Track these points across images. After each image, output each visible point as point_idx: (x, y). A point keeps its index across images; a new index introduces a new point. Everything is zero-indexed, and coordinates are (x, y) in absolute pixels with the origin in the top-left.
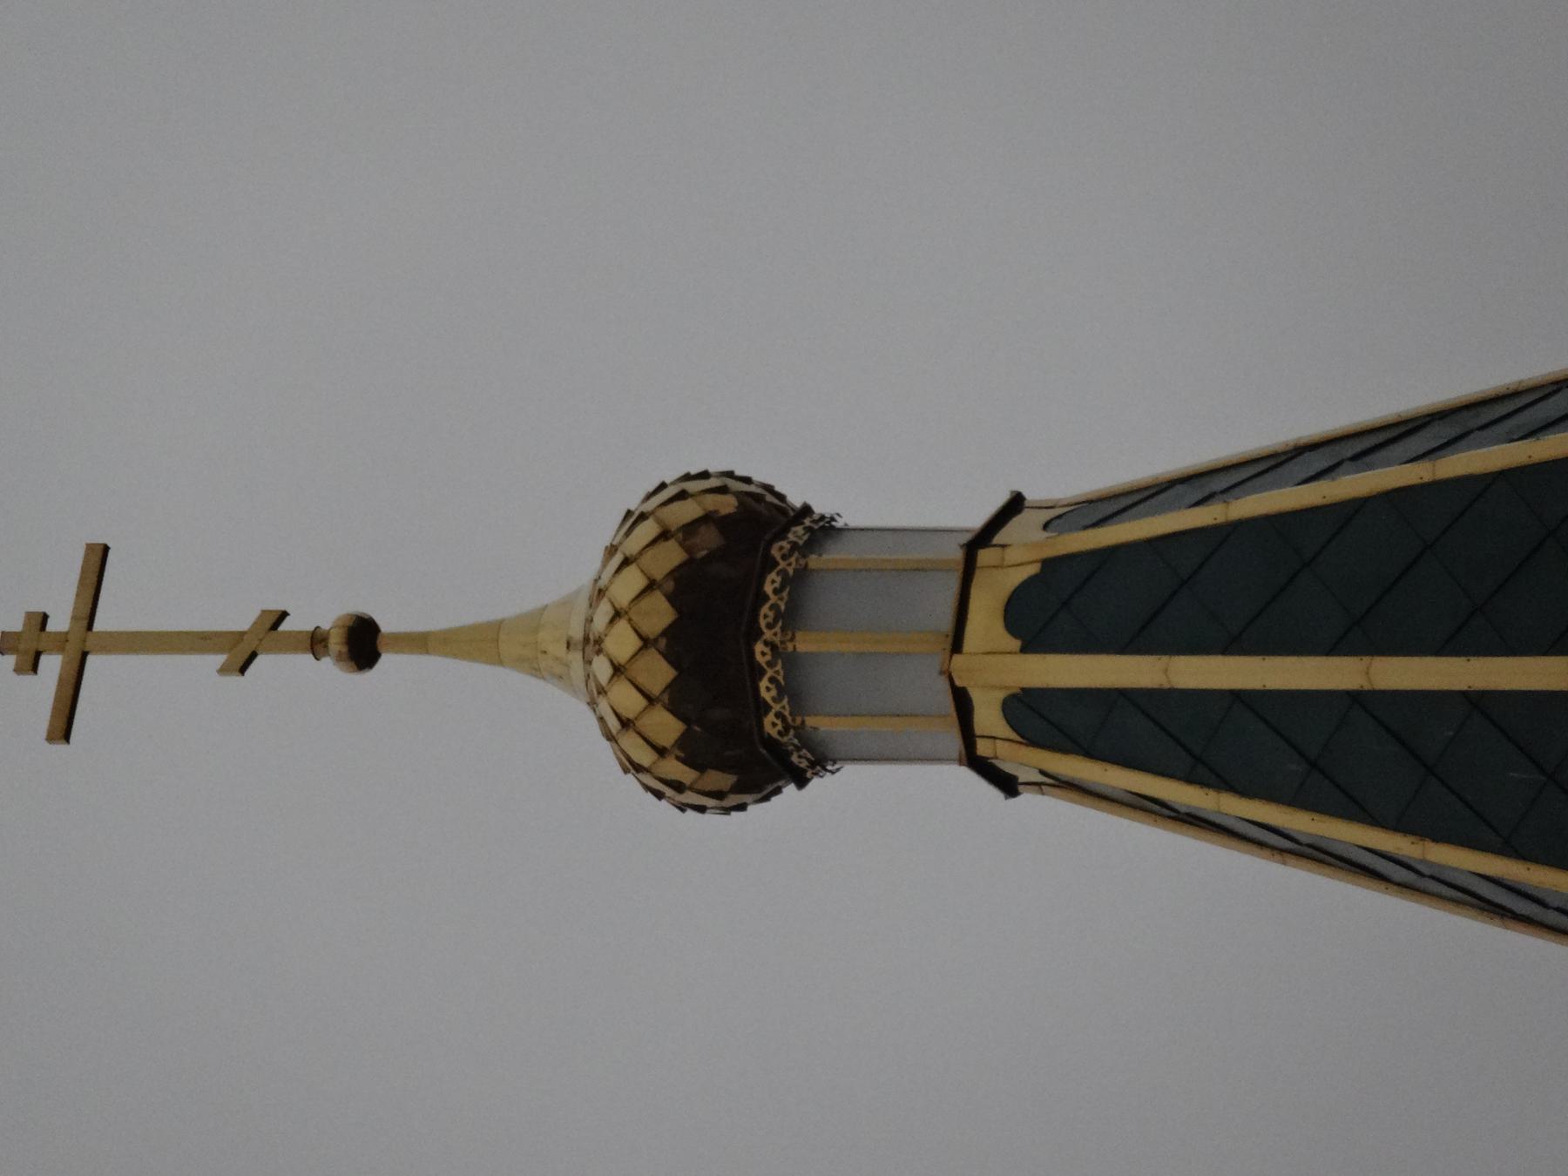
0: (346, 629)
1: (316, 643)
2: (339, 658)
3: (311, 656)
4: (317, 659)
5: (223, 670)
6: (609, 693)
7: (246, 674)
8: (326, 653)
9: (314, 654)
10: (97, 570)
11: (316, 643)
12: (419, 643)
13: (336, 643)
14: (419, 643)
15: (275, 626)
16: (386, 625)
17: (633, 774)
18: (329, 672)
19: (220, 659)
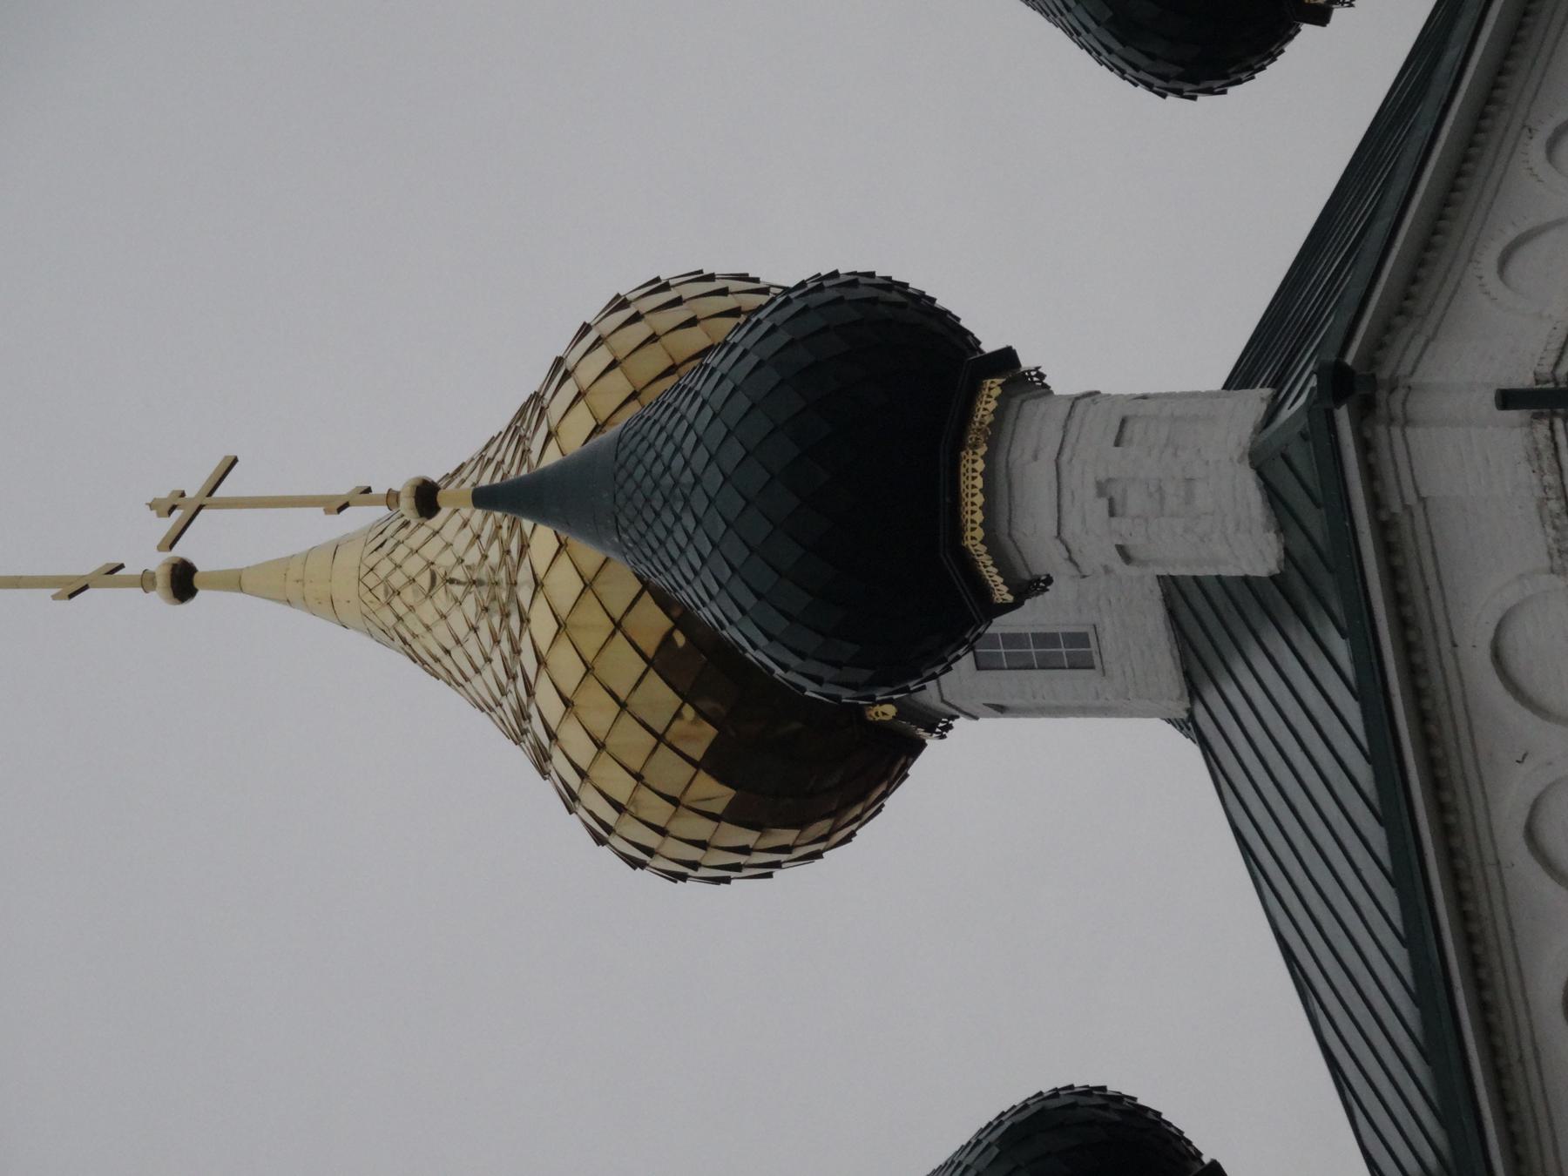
0: (170, 567)
1: (146, 581)
2: (997, 634)
3: (141, 589)
4: (146, 592)
5: (55, 597)
6: (448, 618)
7: (341, 513)
8: (1534, 383)
9: (143, 587)
10: (1364, 1080)
11: (146, 581)
12: (234, 581)
13: (163, 579)
14: (234, 581)
15: (112, 572)
16: (201, 566)
17: (488, 713)
18: (158, 601)
19: (55, 591)
